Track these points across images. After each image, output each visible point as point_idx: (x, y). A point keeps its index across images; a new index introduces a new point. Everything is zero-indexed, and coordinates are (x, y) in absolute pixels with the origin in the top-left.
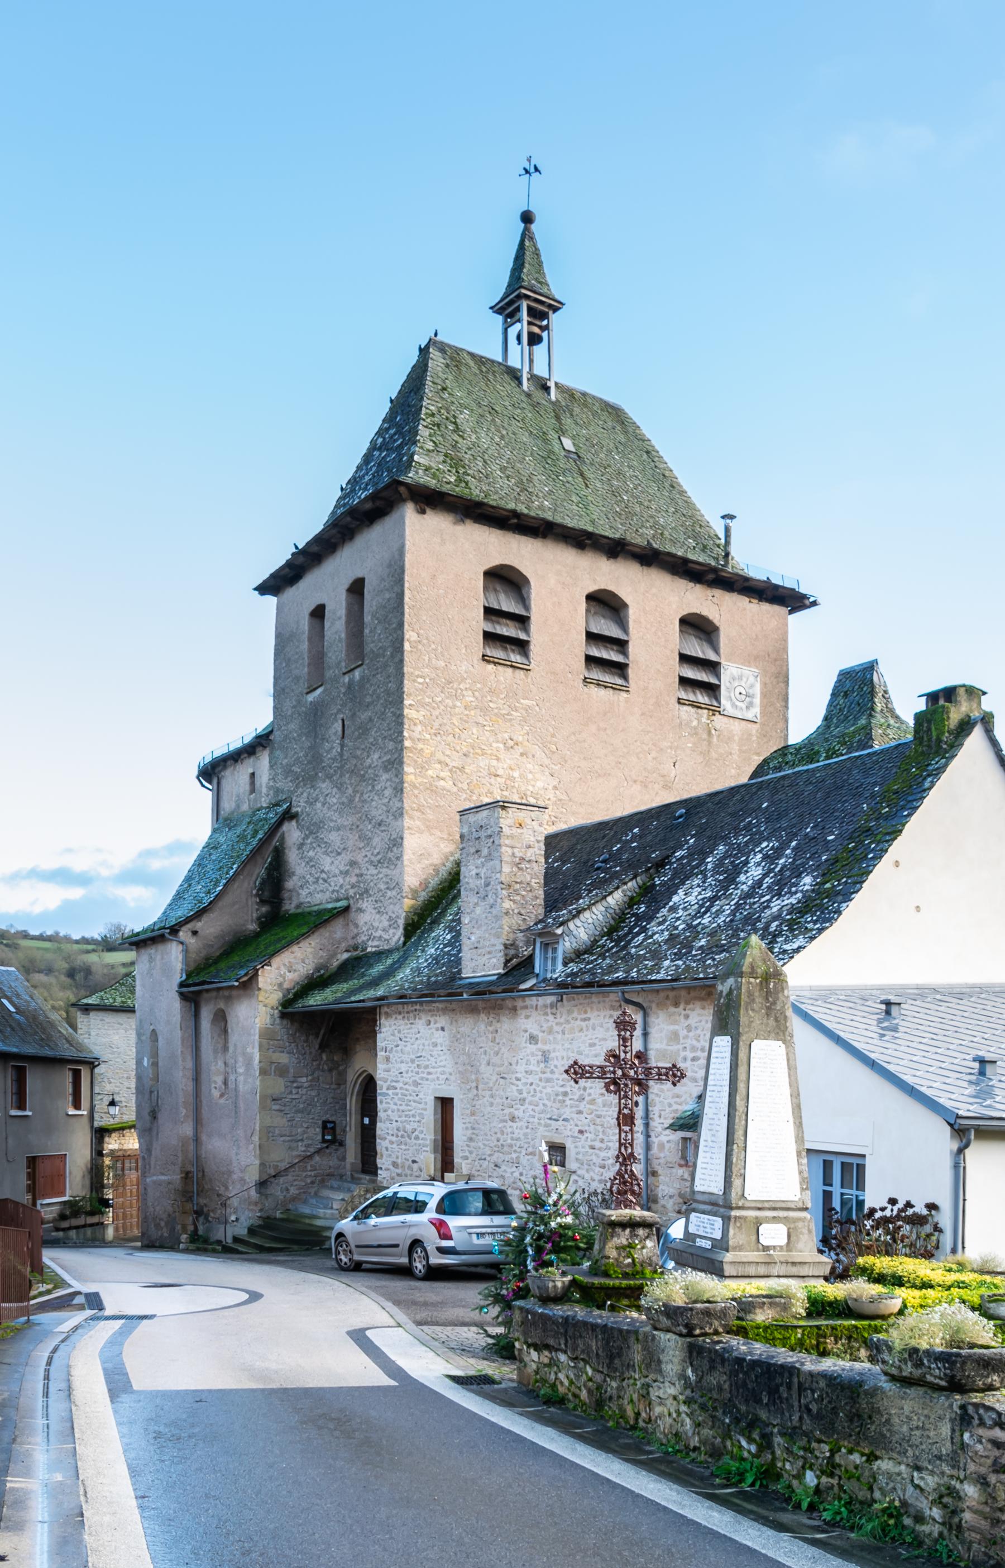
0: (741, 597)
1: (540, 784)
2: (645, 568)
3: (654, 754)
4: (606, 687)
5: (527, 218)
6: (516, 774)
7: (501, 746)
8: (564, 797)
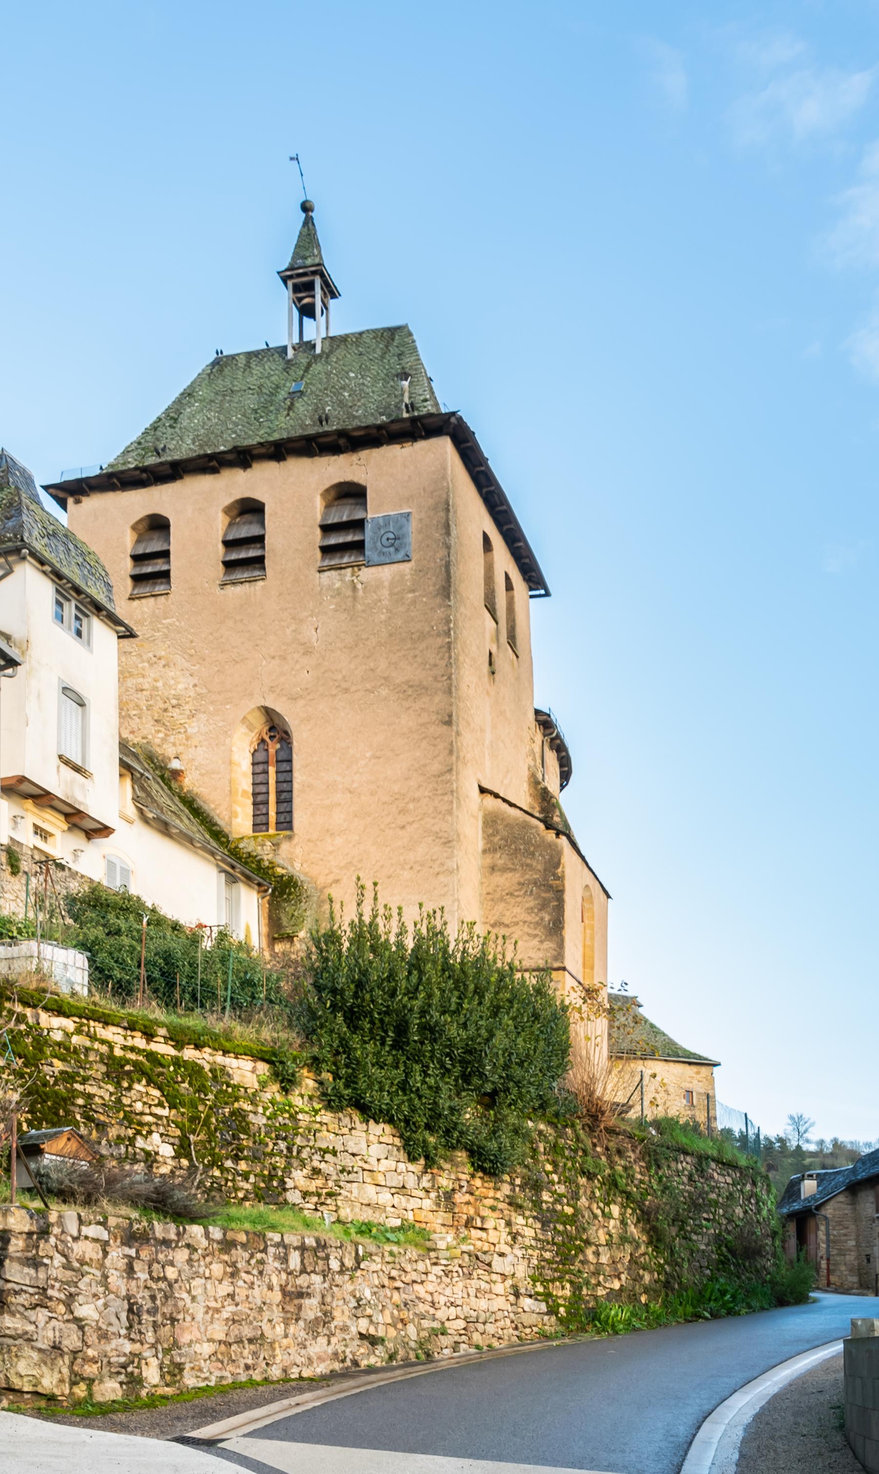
0: (391, 447)
1: (181, 686)
2: (282, 463)
3: (293, 627)
4: (242, 583)
5: (306, 208)
6: (160, 684)
7: (146, 664)
8: (204, 691)
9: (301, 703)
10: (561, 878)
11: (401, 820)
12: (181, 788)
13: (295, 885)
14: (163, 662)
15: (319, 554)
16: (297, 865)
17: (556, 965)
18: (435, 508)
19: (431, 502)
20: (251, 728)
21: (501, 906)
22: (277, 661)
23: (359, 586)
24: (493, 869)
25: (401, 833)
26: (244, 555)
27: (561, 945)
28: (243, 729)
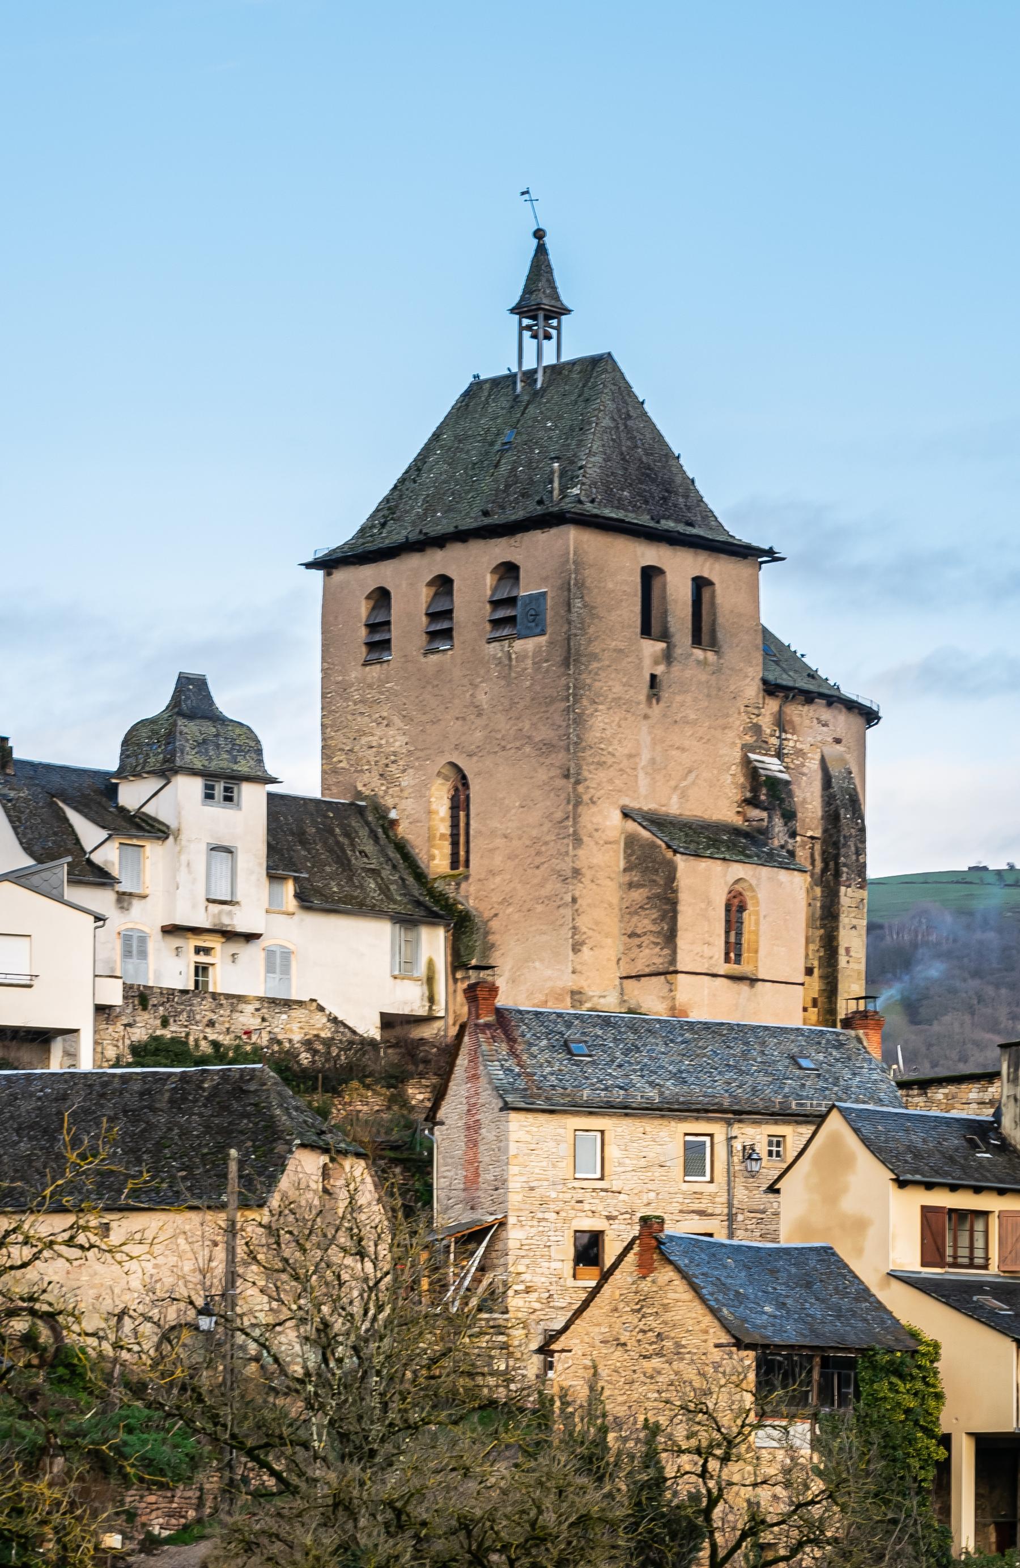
1: (397, 744)
5: (539, 234)
6: (383, 742)
9: (475, 758)
10: (675, 891)
11: (538, 860)
12: (396, 835)
13: (470, 920)
14: (385, 722)
15: (488, 627)
16: (471, 902)
17: (671, 969)
18: (561, 588)
19: (560, 581)
20: (446, 778)
21: (635, 918)
22: (460, 722)
23: (513, 656)
24: (631, 885)
25: (537, 872)
26: (440, 627)
27: (674, 952)
28: (440, 781)
